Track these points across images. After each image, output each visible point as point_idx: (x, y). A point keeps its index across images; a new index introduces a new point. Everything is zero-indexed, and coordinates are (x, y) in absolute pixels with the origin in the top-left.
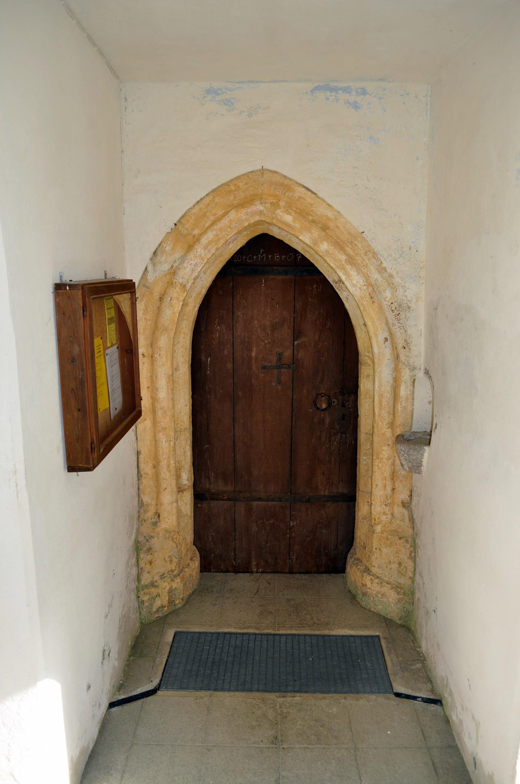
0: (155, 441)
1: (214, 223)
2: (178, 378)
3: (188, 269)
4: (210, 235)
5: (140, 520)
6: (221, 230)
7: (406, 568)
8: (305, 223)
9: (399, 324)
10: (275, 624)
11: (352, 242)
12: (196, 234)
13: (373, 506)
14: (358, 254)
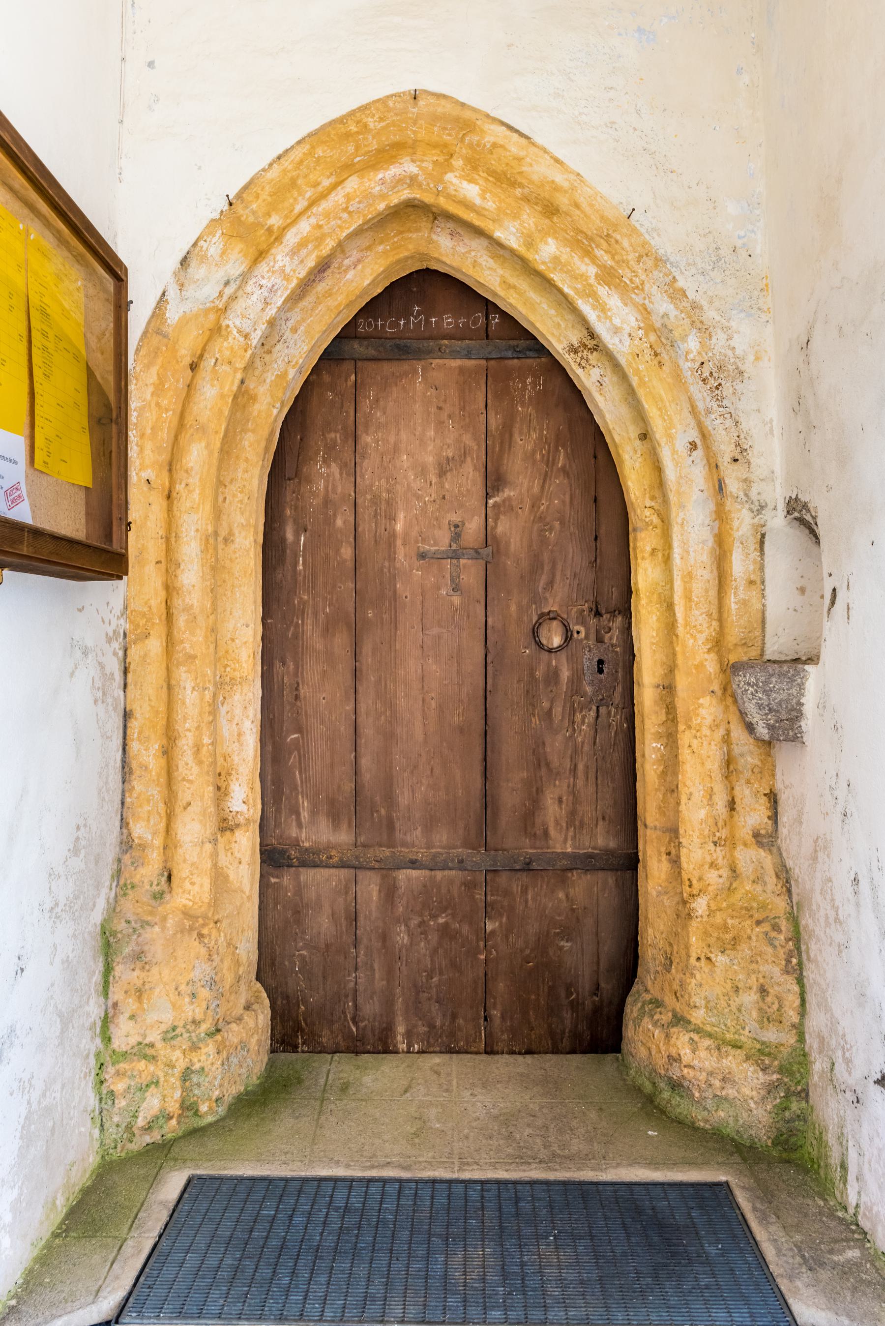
0: (170, 687)
1: (313, 203)
2: (231, 560)
3: (254, 298)
4: (304, 227)
5: (122, 882)
6: (327, 215)
7: (779, 999)
8: (507, 200)
9: (722, 409)
10: (452, 1158)
11: (608, 235)
12: (274, 225)
13: (685, 849)
14: (623, 262)
